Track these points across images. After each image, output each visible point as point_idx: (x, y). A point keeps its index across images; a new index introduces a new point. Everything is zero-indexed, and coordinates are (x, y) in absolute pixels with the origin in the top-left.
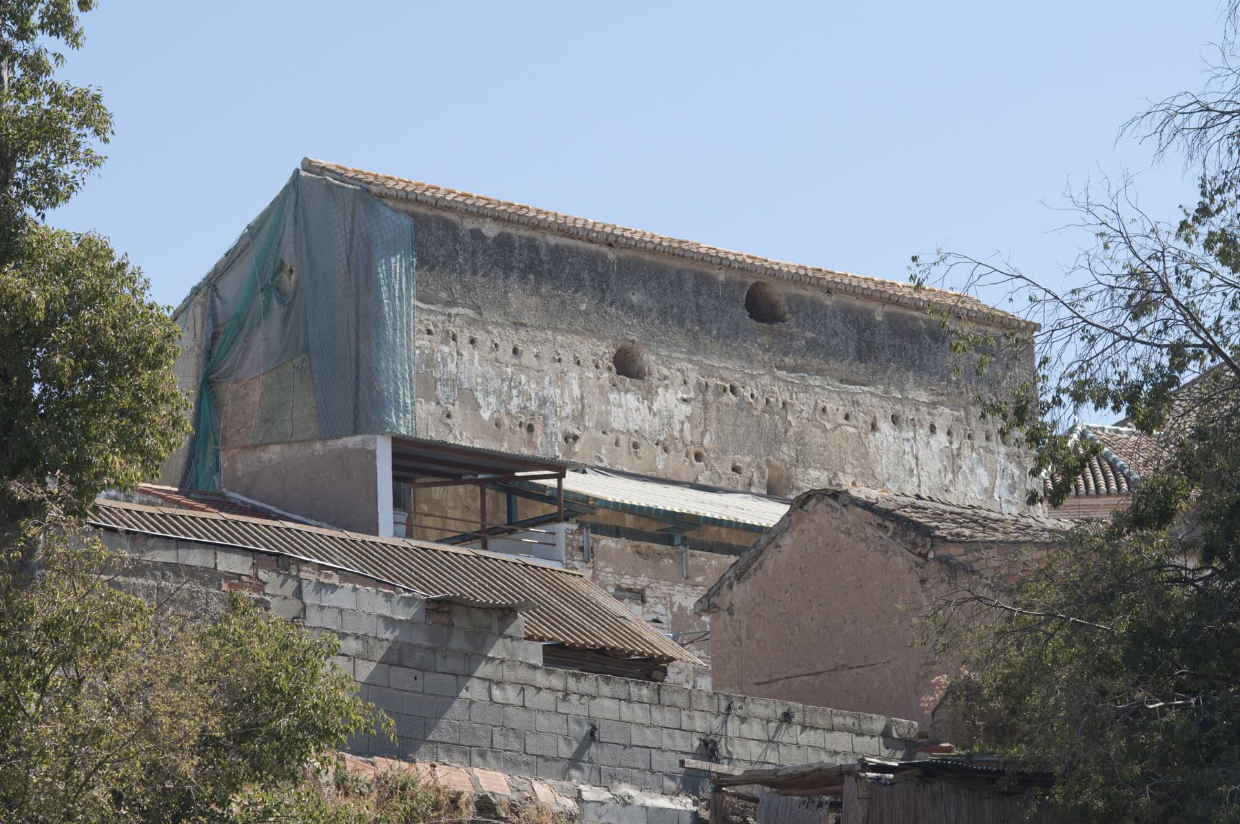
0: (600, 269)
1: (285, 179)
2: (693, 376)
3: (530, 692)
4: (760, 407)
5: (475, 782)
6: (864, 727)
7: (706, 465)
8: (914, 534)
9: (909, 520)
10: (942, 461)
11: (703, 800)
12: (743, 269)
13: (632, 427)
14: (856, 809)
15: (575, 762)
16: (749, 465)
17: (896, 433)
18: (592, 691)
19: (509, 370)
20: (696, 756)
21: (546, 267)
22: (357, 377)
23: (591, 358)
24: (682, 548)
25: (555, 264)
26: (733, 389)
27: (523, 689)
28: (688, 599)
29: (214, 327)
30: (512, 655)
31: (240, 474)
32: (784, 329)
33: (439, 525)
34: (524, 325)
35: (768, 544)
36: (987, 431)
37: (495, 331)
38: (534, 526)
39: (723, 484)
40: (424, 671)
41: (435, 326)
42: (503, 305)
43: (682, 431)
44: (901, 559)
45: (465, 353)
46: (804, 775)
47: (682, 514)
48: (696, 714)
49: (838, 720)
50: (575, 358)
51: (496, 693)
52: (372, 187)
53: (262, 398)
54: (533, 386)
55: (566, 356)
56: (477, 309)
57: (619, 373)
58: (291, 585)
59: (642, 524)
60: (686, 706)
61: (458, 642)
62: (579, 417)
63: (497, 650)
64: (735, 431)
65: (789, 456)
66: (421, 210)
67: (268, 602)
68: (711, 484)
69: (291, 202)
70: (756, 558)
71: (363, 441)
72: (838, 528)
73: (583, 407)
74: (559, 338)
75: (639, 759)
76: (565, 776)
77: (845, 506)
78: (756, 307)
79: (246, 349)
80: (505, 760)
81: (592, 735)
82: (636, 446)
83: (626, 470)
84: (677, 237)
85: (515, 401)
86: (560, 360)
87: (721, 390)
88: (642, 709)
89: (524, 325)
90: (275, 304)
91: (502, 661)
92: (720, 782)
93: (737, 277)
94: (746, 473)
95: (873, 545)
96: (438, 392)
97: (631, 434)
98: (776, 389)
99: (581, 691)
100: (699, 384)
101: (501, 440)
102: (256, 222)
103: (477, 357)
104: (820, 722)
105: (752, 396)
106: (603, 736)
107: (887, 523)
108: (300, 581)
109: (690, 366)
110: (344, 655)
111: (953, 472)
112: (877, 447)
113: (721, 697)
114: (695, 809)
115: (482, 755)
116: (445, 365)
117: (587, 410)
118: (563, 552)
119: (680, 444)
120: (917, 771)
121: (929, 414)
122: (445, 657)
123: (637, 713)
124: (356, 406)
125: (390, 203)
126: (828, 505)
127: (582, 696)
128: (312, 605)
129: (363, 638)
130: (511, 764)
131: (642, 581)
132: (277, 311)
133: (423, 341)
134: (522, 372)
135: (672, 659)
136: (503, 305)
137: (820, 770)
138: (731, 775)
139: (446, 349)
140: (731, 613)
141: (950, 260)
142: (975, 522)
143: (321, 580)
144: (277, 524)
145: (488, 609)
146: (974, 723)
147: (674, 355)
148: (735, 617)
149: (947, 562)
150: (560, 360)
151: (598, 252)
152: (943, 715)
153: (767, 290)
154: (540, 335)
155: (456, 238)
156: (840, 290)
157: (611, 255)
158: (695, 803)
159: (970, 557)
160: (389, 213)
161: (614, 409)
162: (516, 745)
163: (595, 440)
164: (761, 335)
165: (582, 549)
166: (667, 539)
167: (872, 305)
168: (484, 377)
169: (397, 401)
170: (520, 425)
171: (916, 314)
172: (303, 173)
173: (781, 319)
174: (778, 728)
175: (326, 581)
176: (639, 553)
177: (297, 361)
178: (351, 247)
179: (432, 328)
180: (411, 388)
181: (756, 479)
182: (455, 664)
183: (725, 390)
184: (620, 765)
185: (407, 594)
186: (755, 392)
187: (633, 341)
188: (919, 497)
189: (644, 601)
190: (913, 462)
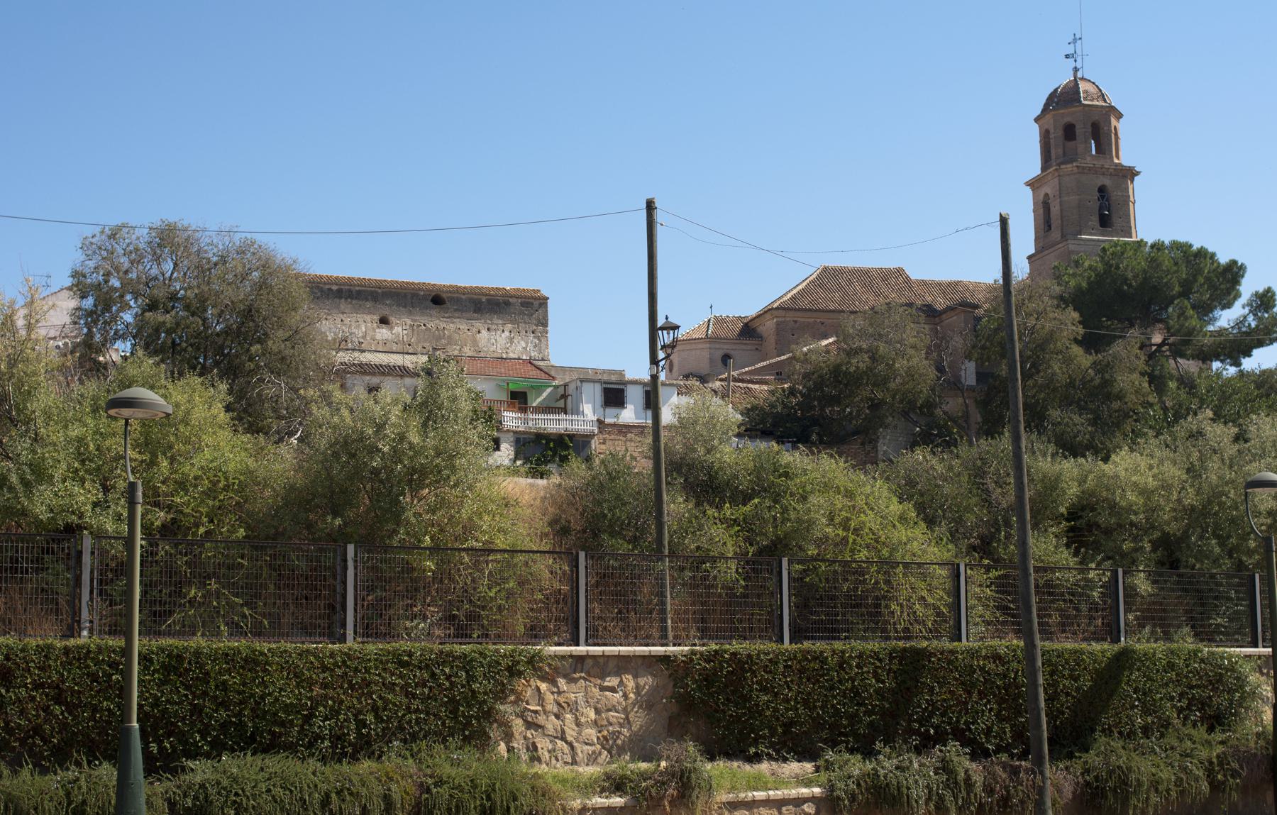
42: (338, 308)
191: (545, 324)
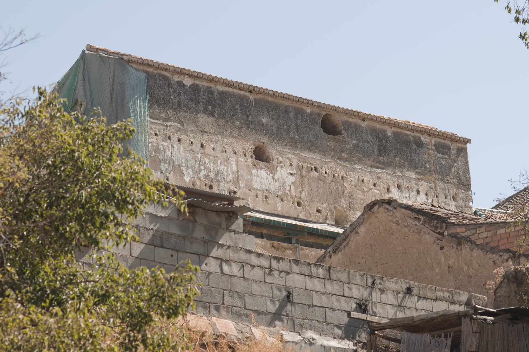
0: (245, 104)
2: (295, 162)
3: (247, 268)
4: (330, 179)
5: (213, 325)
6: (455, 299)
7: (303, 208)
8: (435, 222)
11: (360, 342)
12: (319, 106)
13: (264, 188)
14: (470, 340)
15: (277, 316)
16: (325, 209)
17: (400, 194)
18: (287, 269)
19: (199, 156)
20: (356, 310)
23: (242, 151)
25: (222, 101)
26: (316, 169)
27: (243, 266)
30: (235, 243)
34: (207, 132)
35: (351, 232)
37: (191, 135)
39: (312, 219)
40: (177, 251)
41: (159, 131)
42: (195, 122)
43: (290, 190)
44: (428, 237)
45: (175, 146)
46: (432, 319)
48: (353, 286)
49: (440, 294)
50: (234, 150)
51: (226, 268)
52: (124, 56)
54: (212, 164)
55: (229, 149)
57: (257, 159)
60: (347, 281)
61: (199, 233)
62: (236, 182)
63: (225, 239)
64: (317, 191)
65: (346, 204)
66: (151, 70)
68: (305, 218)
70: (345, 240)
72: (392, 221)
74: (225, 140)
75: (318, 314)
76: (271, 324)
77: (395, 208)
78: (326, 128)
80: (232, 313)
81: (288, 297)
82: (266, 197)
83: (261, 210)
85: (203, 172)
86: (225, 151)
88: (319, 282)
89: (207, 132)
91: (229, 247)
92: (373, 329)
93: (316, 111)
94: (324, 213)
95: (412, 229)
96: (162, 166)
98: (338, 169)
99: (280, 268)
102: (62, 80)
103: (182, 148)
104: (429, 294)
105: (326, 173)
106: (295, 298)
107: (420, 216)
109: (293, 156)
113: (368, 276)
114: (355, 348)
115: (217, 309)
117: (240, 178)
119: (289, 197)
120: (508, 315)
121: (416, 184)
122: (192, 243)
123: (317, 285)
125: (134, 66)
127: (281, 272)
130: (237, 315)
133: (153, 139)
137: (444, 315)
138: (379, 323)
139: (166, 144)
146: (522, 297)
147: (285, 150)
149: (455, 237)
150: (225, 151)
151: (244, 95)
153: (332, 118)
154: (215, 138)
155: (169, 86)
156: (369, 119)
157: (251, 97)
158: (355, 345)
159: (469, 233)
160: (134, 71)
161: (255, 178)
162: (239, 303)
164: (329, 141)
166: (288, 240)
167: (385, 127)
168: (186, 159)
170: (205, 185)
171: (408, 132)
172: (87, 52)
173: (340, 133)
174: (404, 298)
178: (113, 89)
179: (157, 132)
181: (329, 216)
182: (197, 248)
183: (312, 169)
184: (306, 319)
186: (327, 171)
187: (264, 142)
188: (433, 206)
191: (467, 186)
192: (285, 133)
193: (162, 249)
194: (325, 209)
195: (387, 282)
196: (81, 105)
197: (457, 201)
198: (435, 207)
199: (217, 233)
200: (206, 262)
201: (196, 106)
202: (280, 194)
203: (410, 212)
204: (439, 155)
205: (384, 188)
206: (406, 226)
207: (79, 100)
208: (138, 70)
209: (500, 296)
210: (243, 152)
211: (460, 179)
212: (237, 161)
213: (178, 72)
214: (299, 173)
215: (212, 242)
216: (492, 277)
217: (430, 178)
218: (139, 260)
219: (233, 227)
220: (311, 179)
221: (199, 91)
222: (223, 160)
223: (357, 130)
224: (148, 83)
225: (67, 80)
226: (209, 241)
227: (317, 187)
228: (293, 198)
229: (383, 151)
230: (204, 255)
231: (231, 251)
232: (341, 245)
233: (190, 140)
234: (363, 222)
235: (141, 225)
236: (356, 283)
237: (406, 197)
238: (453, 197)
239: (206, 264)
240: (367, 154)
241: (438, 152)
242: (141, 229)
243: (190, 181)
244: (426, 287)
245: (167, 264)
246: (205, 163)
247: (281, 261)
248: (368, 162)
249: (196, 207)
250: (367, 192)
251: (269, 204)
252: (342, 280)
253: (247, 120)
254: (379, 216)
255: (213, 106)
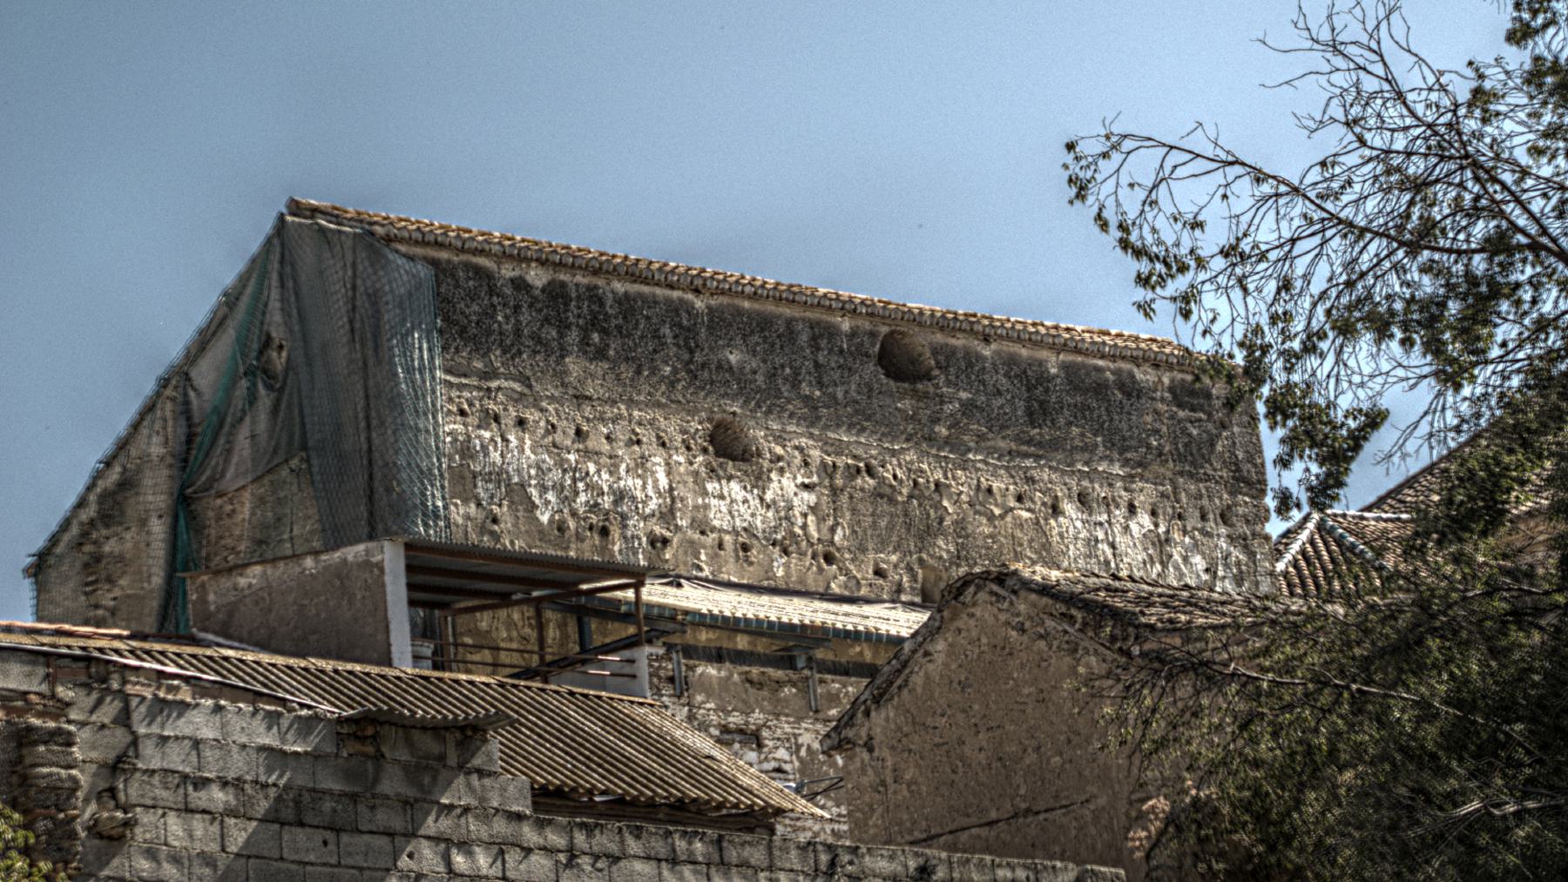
0: (685, 322)
1: (268, 226)
3: (512, 857)
4: (905, 491)
7: (840, 569)
9: (1104, 606)
10: (1145, 549)
12: (872, 315)
16: (896, 566)
18: (613, 848)
19: (572, 457)
21: (614, 322)
22: (371, 477)
23: (679, 438)
24: (807, 672)
25: (625, 318)
27: (502, 852)
28: (810, 736)
29: (190, 426)
30: (482, 800)
31: (212, 608)
32: (931, 390)
33: (489, 659)
34: (590, 398)
36: (1202, 508)
38: (607, 653)
40: (338, 831)
41: (471, 405)
42: (560, 376)
43: (804, 527)
45: (512, 438)
47: (803, 626)
50: (658, 437)
51: (459, 860)
53: (253, 514)
54: (605, 476)
56: (525, 381)
58: (109, 710)
59: (762, 646)
61: (392, 784)
63: (456, 794)
64: (874, 522)
65: (948, 552)
66: (444, 255)
67: (70, 733)
68: (847, 593)
69: (276, 257)
70: (899, 671)
71: (367, 551)
72: (1008, 623)
73: (673, 500)
74: (636, 413)
77: (1015, 592)
79: (229, 452)
82: (745, 548)
83: (734, 579)
84: (786, 281)
85: (582, 498)
86: (639, 442)
87: (853, 471)
88: (696, 872)
90: (262, 390)
91: (466, 810)
93: (866, 325)
95: (1056, 643)
97: (737, 534)
98: (925, 466)
99: (596, 849)
100: (824, 464)
101: (567, 548)
103: (528, 442)
105: (895, 477)
107: (1074, 612)
108: (126, 698)
109: (811, 442)
110: (204, 812)
111: (1162, 563)
112: (1061, 535)
113: (820, 848)
116: (486, 454)
118: (647, 686)
121: (1126, 489)
122: (373, 808)
124: (371, 514)
125: (403, 248)
126: (992, 593)
128: (148, 736)
129: (237, 784)
131: (757, 717)
132: (265, 399)
134: (590, 459)
135: (780, 812)
136: (560, 376)
139: (487, 435)
140: (871, 750)
141: (1128, 145)
142: (1196, 605)
143: (162, 694)
144: (209, 652)
145: (438, 729)
146: (1210, 867)
148: (876, 754)
150: (639, 442)
151: (681, 300)
152: (1162, 857)
154: (610, 412)
155: (492, 291)
156: (1001, 337)
160: (401, 261)
161: (714, 502)
163: (691, 542)
164: (900, 399)
165: (671, 680)
166: (787, 662)
167: (1043, 354)
169: (424, 504)
171: (1101, 363)
175: (170, 697)
176: (750, 682)
177: (294, 463)
178: (354, 308)
179: (466, 407)
180: (443, 487)
185: (304, 712)
187: (734, 413)
189: (760, 746)
190: (1109, 552)
192: (788, 386)
193: (299, 830)
194: (896, 566)
195: (867, 858)
196: (281, 347)
197: (1232, 526)
198: (1120, 579)
199: (434, 779)
200: (408, 849)
201: (561, 335)
202: (779, 537)
203: (1051, 602)
204: (1181, 414)
205: (1044, 504)
206: (1041, 637)
207: (274, 335)
208: (411, 258)
209: (1157, 868)
210: (684, 441)
211: (1238, 470)
212: (668, 464)
213: (511, 256)
214: (827, 482)
215: (425, 800)
216: (1141, 819)
217: (1162, 470)
218: (243, 861)
219: (477, 761)
220: (859, 495)
221: (567, 300)
222: (632, 465)
223: (970, 365)
224: (438, 286)
225: (244, 287)
226: (416, 800)
227: (873, 515)
228: (812, 545)
229: (1039, 412)
230: (405, 835)
231: (471, 820)
232: (892, 683)
233: (548, 422)
234: (939, 628)
235: (248, 778)
236: (788, 866)
237: (1101, 524)
238: (1222, 516)
239: (410, 856)
240: (999, 424)
241: (1180, 406)
242: (247, 786)
243: (551, 521)
244: (968, 861)
245: (312, 864)
246: (587, 474)
247: (597, 832)
248: (1002, 444)
249: (381, 724)
250: (1002, 517)
251: (751, 564)
252: (753, 861)
253: (691, 361)
254: (978, 612)
255: (604, 332)
